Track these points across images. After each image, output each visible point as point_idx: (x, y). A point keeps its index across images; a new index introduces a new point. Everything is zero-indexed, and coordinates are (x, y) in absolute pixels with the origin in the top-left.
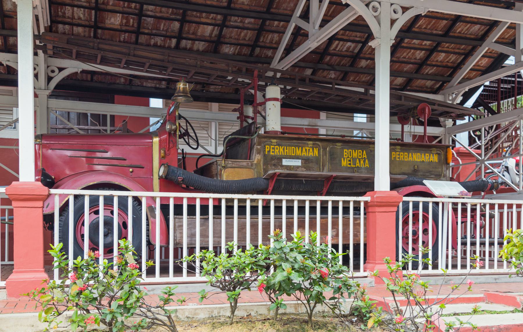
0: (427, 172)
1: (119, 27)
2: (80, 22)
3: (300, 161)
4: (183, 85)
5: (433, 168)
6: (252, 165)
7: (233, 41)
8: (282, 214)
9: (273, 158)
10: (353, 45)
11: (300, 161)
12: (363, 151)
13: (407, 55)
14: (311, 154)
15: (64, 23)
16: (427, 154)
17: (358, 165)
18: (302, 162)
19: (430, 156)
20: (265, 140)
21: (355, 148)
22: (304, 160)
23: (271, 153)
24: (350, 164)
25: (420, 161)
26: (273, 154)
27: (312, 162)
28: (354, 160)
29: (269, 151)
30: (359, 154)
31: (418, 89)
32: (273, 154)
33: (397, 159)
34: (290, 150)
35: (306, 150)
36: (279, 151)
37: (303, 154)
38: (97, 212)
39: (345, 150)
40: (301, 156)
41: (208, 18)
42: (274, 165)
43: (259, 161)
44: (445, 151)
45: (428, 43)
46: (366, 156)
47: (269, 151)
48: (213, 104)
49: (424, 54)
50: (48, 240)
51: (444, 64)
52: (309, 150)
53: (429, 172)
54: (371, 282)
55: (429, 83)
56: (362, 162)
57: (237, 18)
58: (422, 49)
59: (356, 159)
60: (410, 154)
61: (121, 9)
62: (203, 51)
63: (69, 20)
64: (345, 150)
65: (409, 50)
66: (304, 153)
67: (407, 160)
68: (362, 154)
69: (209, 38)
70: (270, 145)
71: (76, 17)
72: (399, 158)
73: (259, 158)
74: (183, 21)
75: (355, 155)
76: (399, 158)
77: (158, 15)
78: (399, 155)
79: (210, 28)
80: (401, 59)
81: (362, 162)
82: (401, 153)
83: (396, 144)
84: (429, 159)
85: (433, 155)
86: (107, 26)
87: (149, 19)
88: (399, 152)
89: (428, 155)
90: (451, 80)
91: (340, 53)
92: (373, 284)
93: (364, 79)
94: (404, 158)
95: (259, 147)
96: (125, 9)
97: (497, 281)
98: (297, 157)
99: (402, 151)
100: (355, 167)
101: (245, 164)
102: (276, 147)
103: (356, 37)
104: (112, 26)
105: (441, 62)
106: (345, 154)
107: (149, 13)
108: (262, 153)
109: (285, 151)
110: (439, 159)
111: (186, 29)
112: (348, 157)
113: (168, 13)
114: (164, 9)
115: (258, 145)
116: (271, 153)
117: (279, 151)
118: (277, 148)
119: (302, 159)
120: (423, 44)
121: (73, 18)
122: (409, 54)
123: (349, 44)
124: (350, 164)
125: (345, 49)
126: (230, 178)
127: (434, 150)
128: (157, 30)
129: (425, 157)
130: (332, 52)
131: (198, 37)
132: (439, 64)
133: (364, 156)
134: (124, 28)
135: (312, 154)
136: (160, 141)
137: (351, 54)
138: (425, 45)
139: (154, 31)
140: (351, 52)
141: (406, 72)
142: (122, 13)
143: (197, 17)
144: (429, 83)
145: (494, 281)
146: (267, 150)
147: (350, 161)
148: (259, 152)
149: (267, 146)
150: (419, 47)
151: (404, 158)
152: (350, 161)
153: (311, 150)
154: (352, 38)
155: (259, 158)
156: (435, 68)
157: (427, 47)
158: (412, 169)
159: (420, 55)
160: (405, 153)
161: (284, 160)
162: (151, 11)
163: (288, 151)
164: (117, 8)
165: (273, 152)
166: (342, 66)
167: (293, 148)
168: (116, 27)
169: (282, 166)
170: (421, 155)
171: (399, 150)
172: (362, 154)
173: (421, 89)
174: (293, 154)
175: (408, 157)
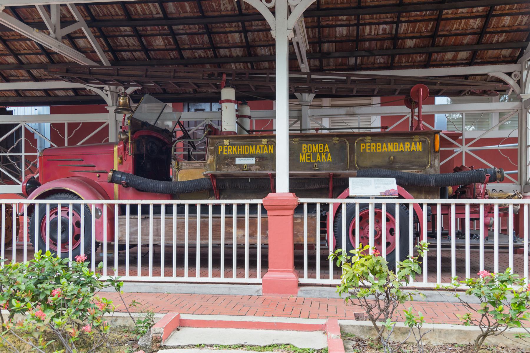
0: (408, 163)
1: (164, 47)
2: (134, 48)
3: (254, 159)
4: (123, 99)
5: (415, 158)
6: (205, 166)
7: (263, 43)
8: (208, 213)
9: (226, 157)
10: (388, 27)
11: (254, 159)
12: (324, 145)
13: (459, 25)
14: (265, 151)
15: (125, 51)
16: (406, 143)
17: (318, 159)
18: (256, 160)
19: (411, 144)
20: (218, 140)
21: (315, 143)
22: (259, 157)
23: (224, 153)
24: (309, 159)
25: (398, 152)
26: (226, 154)
27: (267, 159)
28: (314, 155)
29: (222, 152)
30: (320, 148)
31: (492, 60)
32: (226, 154)
33: (367, 151)
34: (243, 149)
35: (260, 148)
36: (232, 151)
37: (257, 151)
38: (56, 214)
39: (303, 145)
40: (255, 154)
41: (231, 27)
42: (227, 164)
43: (212, 161)
44: (432, 137)
45: (480, 9)
46: (328, 150)
47: (222, 152)
48: (324, 99)
49: (481, 21)
50: (265, 247)
51: (515, 28)
52: (264, 148)
53: (411, 162)
54: (258, 291)
55: (505, 52)
56: (323, 156)
57: (257, 22)
58: (475, 17)
59: (316, 153)
60: (385, 145)
61: (158, 32)
62: (242, 56)
63: (126, 48)
64: (303, 145)
65: (459, 21)
66: (258, 151)
67: (380, 151)
68: (324, 148)
69: (240, 44)
70: (223, 145)
71: (131, 45)
72: (370, 149)
73: (212, 158)
74: (210, 33)
75: (315, 149)
76: (370, 149)
77: (188, 32)
78: (370, 146)
79: (237, 35)
80: (453, 32)
81: (323, 156)
82: (372, 144)
83: (298, 138)
84: (410, 148)
85: (415, 144)
86: (156, 48)
87: (184, 37)
88: (371, 143)
89: (409, 143)
90: (528, 45)
91: (376, 37)
92: (261, 293)
93: (419, 59)
94: (376, 149)
95: (212, 148)
96: (161, 32)
97: (429, 299)
98: (251, 156)
99: (373, 141)
100: (316, 162)
101: (198, 165)
102: (229, 147)
103: (387, 18)
104: (158, 47)
105: (509, 26)
106: (303, 149)
107: (181, 31)
108: (215, 154)
109: (239, 150)
110: (424, 148)
111: (218, 39)
112: (307, 152)
113: (196, 29)
114: (191, 26)
115: (211, 146)
116: (224, 153)
117: (232, 151)
118: (230, 148)
119: (256, 158)
120: (474, 11)
121: (129, 46)
122: (462, 25)
123: (382, 27)
124: (309, 159)
125: (381, 32)
126: (184, 179)
127: (417, 138)
128: (195, 44)
129: (404, 146)
130: (368, 37)
131: (230, 45)
132: (508, 29)
133: (325, 150)
134: (168, 47)
135: (267, 151)
136: (118, 149)
137: (389, 36)
138: (478, 11)
139: (193, 46)
140: (388, 34)
141: (467, 44)
142: (160, 35)
143: (222, 27)
144: (505, 52)
145: (424, 299)
146: (220, 150)
147: (308, 156)
148: (212, 154)
149: (219, 147)
150: (469, 15)
151: (376, 149)
152: (308, 156)
153: (266, 147)
154: (382, 20)
155: (212, 158)
156: (504, 34)
157: (481, 14)
158: (387, 159)
159: (476, 23)
160: (378, 144)
161: (237, 159)
162: (182, 29)
163: (241, 150)
164: (155, 32)
165: (226, 152)
166: (386, 49)
167: (246, 146)
168: (162, 48)
169: (235, 165)
170: (399, 144)
171: (369, 141)
172: (324, 148)
173: (496, 60)
174: (246, 153)
175: (382, 147)
